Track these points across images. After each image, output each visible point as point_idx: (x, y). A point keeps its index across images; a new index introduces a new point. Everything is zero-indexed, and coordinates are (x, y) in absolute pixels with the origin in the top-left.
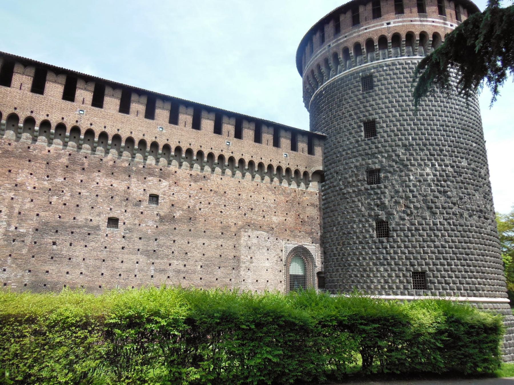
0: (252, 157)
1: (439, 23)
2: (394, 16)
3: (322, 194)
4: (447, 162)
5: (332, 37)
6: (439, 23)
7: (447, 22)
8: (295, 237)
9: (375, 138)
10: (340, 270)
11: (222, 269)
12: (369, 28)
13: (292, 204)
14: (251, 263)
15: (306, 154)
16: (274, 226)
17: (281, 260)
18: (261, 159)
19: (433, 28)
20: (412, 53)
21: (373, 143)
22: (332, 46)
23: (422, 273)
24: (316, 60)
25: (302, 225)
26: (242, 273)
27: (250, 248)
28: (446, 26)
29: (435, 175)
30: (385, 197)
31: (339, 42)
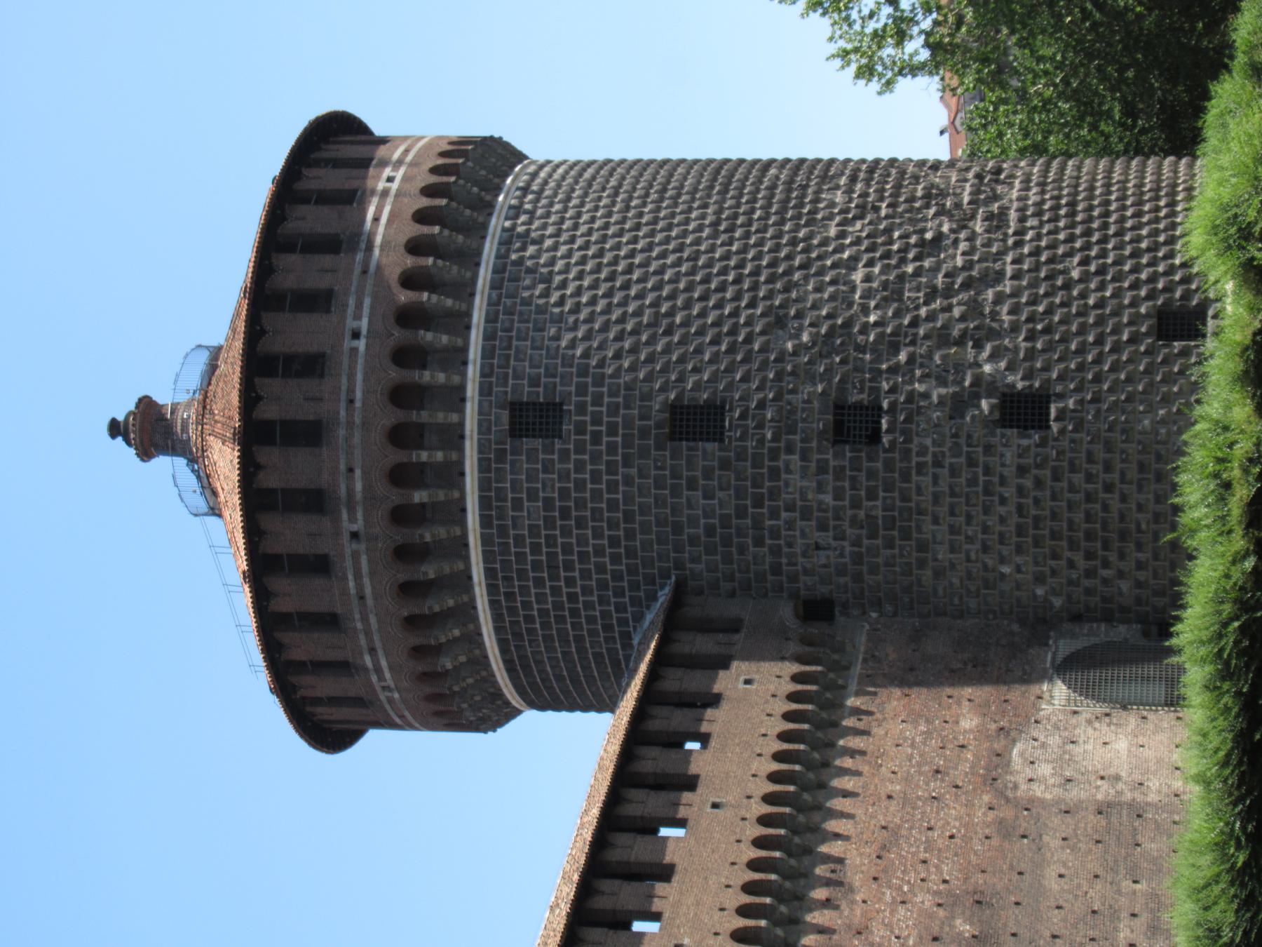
0: (760, 755)
4: (833, 232)
11: (1140, 839)
12: (351, 390)
15: (736, 637)
16: (993, 726)
18: (764, 735)
22: (358, 526)
23: (1160, 319)
26: (1152, 798)
31: (359, 496)
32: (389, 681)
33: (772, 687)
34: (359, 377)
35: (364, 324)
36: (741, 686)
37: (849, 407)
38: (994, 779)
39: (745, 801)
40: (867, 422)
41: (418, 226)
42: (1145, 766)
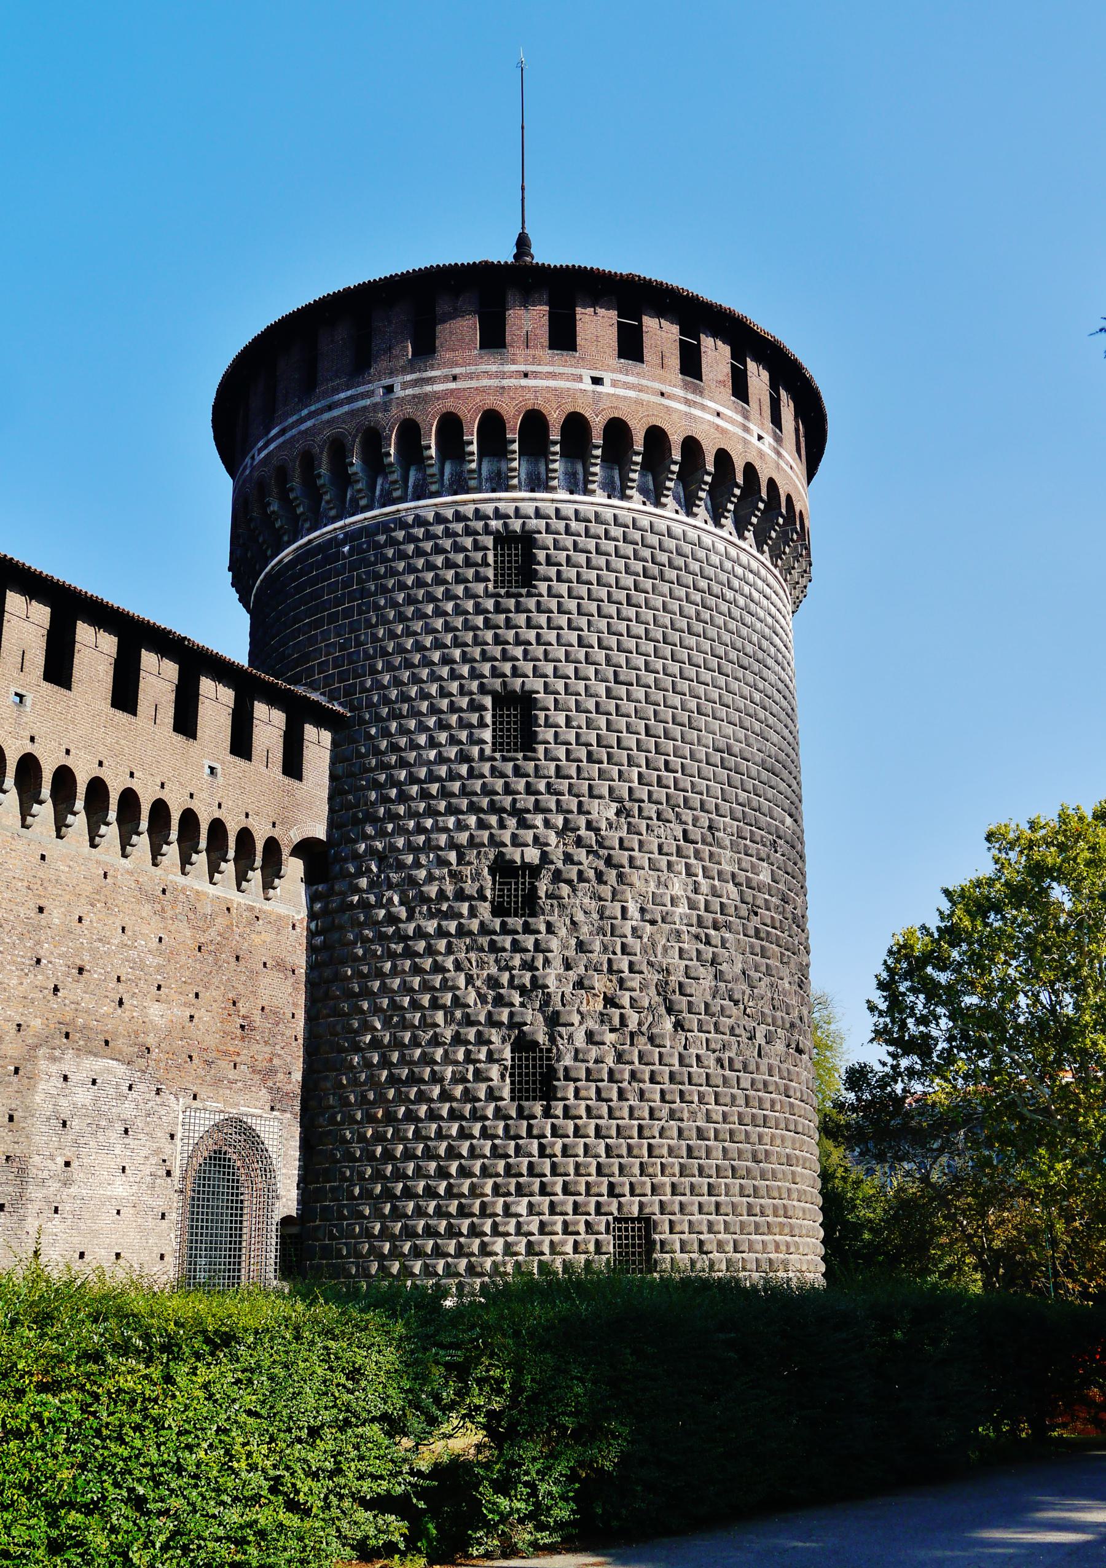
0: (101, 764)
1: (732, 421)
4: (727, 868)
6: (732, 421)
7: (751, 426)
9: (525, 758)
12: (536, 375)
14: (67, 1183)
16: (151, 1041)
17: (169, 1174)
18: (132, 775)
19: (718, 435)
21: (518, 772)
22: (399, 392)
24: (330, 422)
27: (64, 1124)
29: (692, 906)
30: (547, 962)
31: (428, 388)
34: (552, 383)
36: (207, 763)
38: (67, 1035)
39: (28, 734)
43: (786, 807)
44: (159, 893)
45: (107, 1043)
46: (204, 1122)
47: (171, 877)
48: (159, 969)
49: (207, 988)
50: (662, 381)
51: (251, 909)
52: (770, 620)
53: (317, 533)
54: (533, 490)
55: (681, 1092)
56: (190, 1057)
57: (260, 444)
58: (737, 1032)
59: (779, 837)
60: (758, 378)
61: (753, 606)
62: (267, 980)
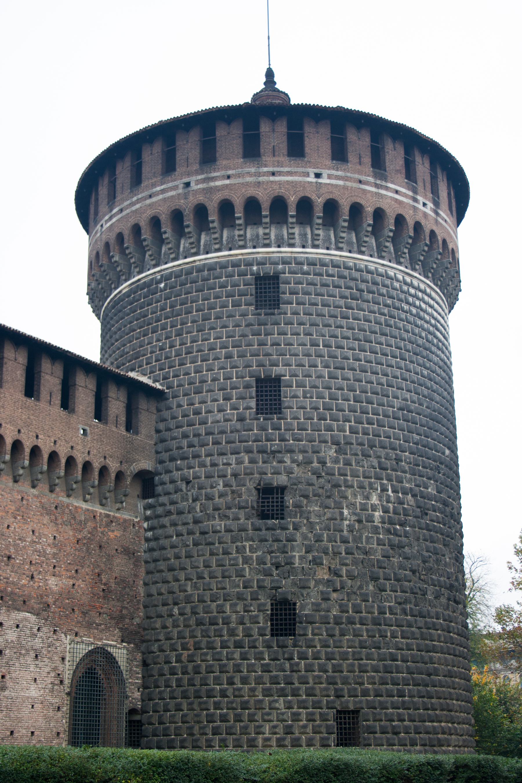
0: (19, 431)
2: (329, 162)
3: (145, 525)
5: (196, 167)
7: (419, 197)
8: (89, 625)
9: (279, 419)
10: (185, 706)
12: (280, 173)
13: (88, 549)
15: (122, 430)
16: (50, 600)
17: (61, 682)
18: (37, 437)
19: (397, 205)
20: (356, 248)
22: (194, 187)
25: (104, 598)
28: (416, 204)
31: (212, 184)
32: (105, 227)
33: (79, 447)
35: (324, 180)
37: (282, 498)
40: (273, 510)
41: (394, 217)
42: (14, 709)
43: (446, 443)
44: (53, 509)
45: (24, 602)
46: (83, 650)
47: (61, 498)
48: (54, 555)
49: (83, 567)
50: (360, 173)
51: (108, 516)
52: (433, 321)
53: (144, 275)
54: (279, 246)
55: (380, 631)
56: (73, 610)
57: (107, 217)
58: (415, 591)
59: (441, 463)
60: (423, 167)
61: (422, 313)
62: (118, 561)
